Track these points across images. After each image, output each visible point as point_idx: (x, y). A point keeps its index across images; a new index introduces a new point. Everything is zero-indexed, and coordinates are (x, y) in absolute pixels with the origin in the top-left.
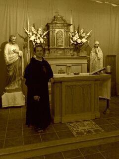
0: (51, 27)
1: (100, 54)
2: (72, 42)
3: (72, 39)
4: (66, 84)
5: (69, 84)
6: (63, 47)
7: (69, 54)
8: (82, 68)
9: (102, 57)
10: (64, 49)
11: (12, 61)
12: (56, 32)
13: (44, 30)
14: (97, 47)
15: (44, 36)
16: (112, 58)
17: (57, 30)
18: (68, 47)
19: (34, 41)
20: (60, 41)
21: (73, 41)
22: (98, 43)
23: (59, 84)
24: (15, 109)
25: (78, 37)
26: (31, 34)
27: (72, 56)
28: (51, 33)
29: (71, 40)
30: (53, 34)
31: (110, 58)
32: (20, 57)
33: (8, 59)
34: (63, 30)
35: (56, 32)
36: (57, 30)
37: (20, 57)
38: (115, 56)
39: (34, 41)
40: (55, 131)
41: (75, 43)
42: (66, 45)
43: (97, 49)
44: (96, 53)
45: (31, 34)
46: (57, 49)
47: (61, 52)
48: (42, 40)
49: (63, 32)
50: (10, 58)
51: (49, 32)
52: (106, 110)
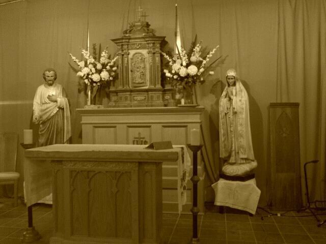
1: (240, 99)
4: (70, 166)
5: (79, 167)
6: (146, 88)
7: (158, 102)
8: (151, 131)
10: (147, 91)
14: (234, 84)
15: (112, 67)
16: (288, 110)
17: (132, 52)
19: (87, 78)
20: (137, 74)
21: (170, 72)
22: (231, 73)
24: (170, 191)
26: (82, 64)
27: (165, 106)
31: (279, 111)
32: (61, 109)
34: (144, 52)
35: (130, 56)
36: (132, 52)
37: (61, 109)
38: (296, 105)
39: (87, 78)
40: (276, 224)
44: (230, 99)
45: (82, 64)
46: (131, 91)
47: (140, 97)
52: (192, 240)
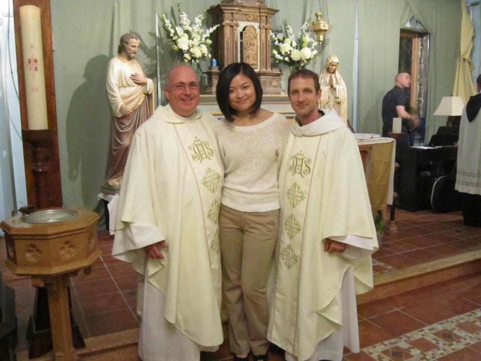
0: (226, 16)
2: (278, 56)
3: (278, 48)
9: (346, 96)
11: (130, 108)
12: (240, 29)
13: (207, 24)
14: (334, 72)
18: (269, 70)
21: (280, 53)
23: (289, 342)
25: (294, 44)
28: (227, 30)
29: (275, 52)
30: (233, 34)
32: (148, 96)
33: (121, 103)
34: (256, 25)
37: (148, 96)
41: (287, 59)
42: (264, 64)
43: (333, 75)
48: (205, 50)
49: (258, 30)
50: (124, 98)
51: (222, 27)
